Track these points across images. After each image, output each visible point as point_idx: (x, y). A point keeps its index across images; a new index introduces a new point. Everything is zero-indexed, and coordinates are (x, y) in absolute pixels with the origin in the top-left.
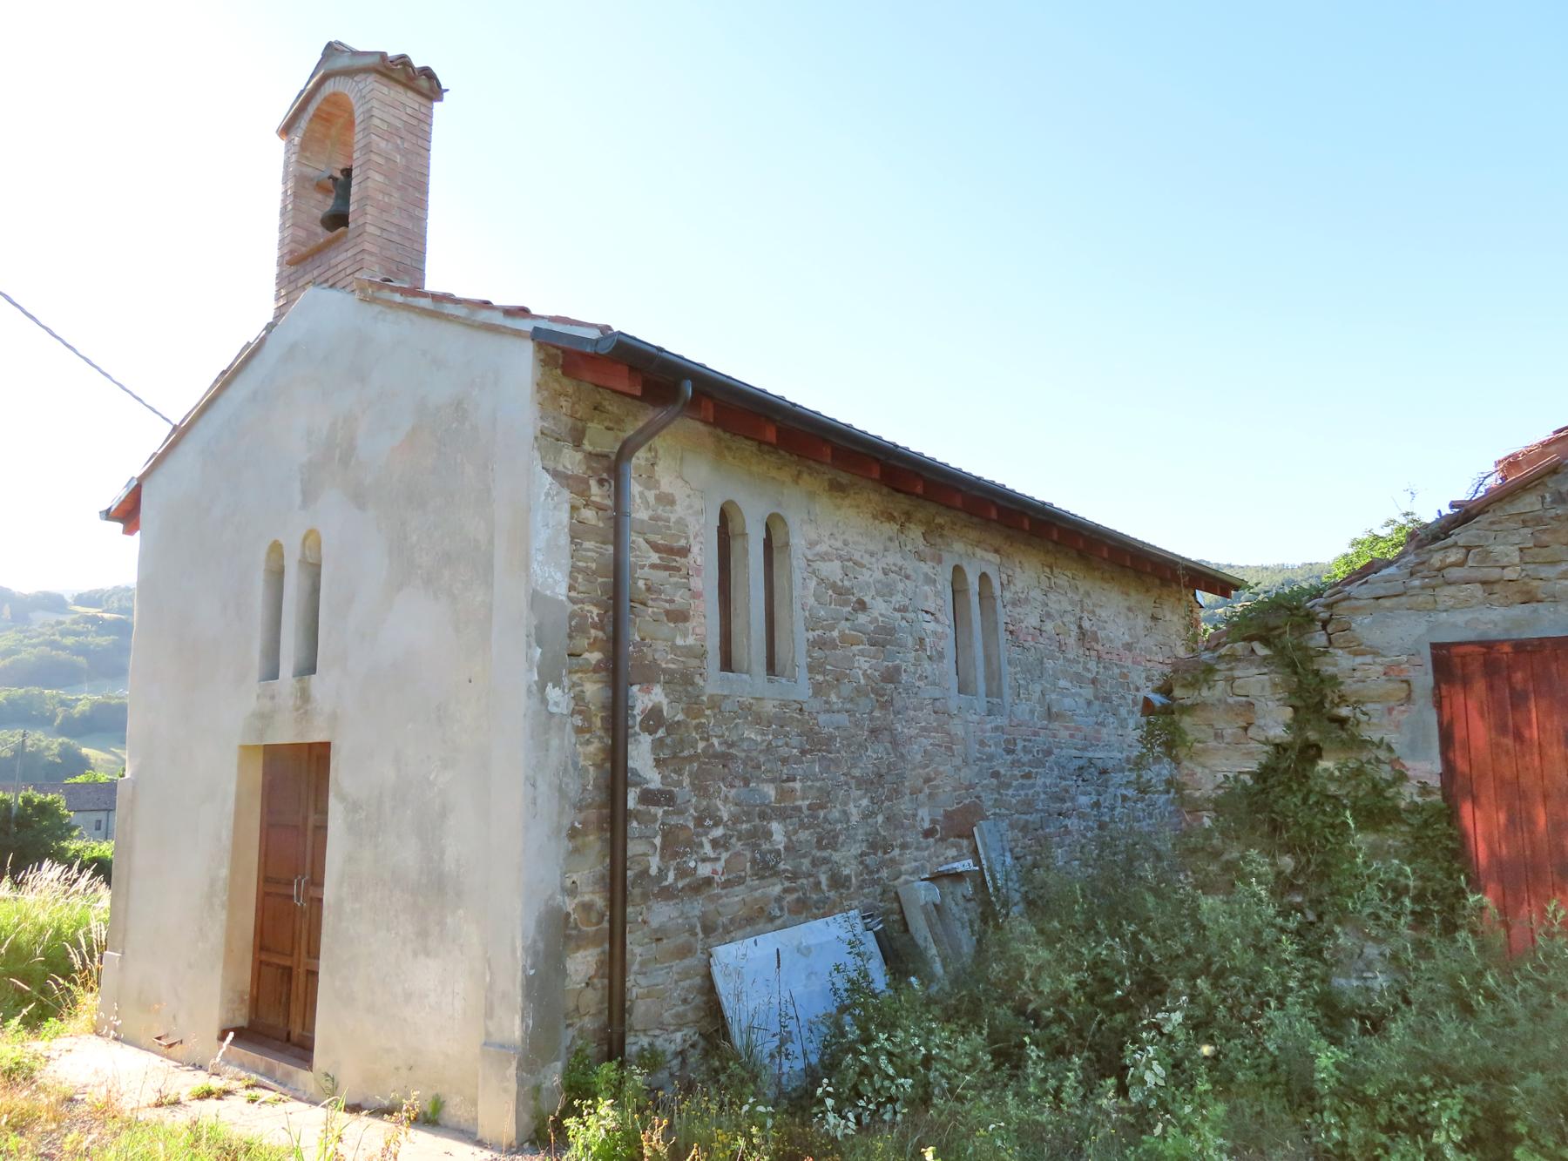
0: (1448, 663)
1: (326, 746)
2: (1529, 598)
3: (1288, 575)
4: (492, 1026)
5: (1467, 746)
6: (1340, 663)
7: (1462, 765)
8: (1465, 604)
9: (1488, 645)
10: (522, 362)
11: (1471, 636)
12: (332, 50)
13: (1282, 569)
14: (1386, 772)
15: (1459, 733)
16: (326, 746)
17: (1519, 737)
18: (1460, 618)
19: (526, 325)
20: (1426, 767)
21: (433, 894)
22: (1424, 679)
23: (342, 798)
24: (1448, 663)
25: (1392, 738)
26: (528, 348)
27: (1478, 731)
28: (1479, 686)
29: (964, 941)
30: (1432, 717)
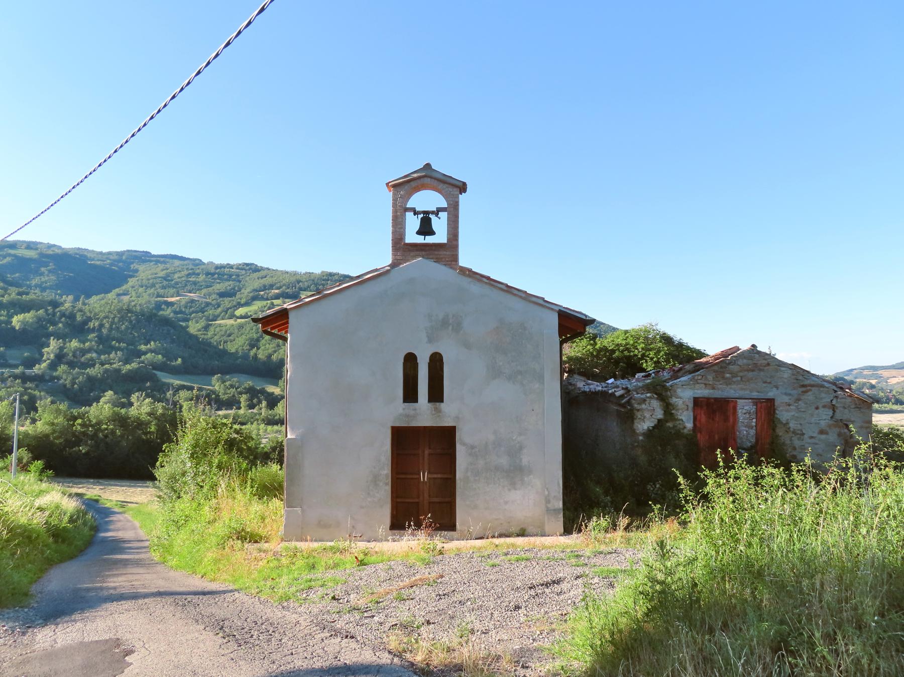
0: (697, 402)
1: (455, 427)
2: (713, 388)
3: (298, 277)
4: (549, 506)
5: (700, 421)
6: (674, 400)
7: (698, 425)
8: (701, 389)
9: (708, 399)
10: (554, 320)
11: (701, 396)
12: (428, 166)
13: (295, 274)
14: (681, 427)
15: (698, 417)
16: (455, 427)
17: (713, 420)
18: (699, 392)
19: (557, 308)
20: (689, 425)
21: (515, 473)
22: (691, 405)
23: (464, 444)
24: (697, 402)
25: (684, 419)
26: (557, 315)
27: (703, 418)
28: (705, 408)
29: (45, 499)
30: (692, 414)
